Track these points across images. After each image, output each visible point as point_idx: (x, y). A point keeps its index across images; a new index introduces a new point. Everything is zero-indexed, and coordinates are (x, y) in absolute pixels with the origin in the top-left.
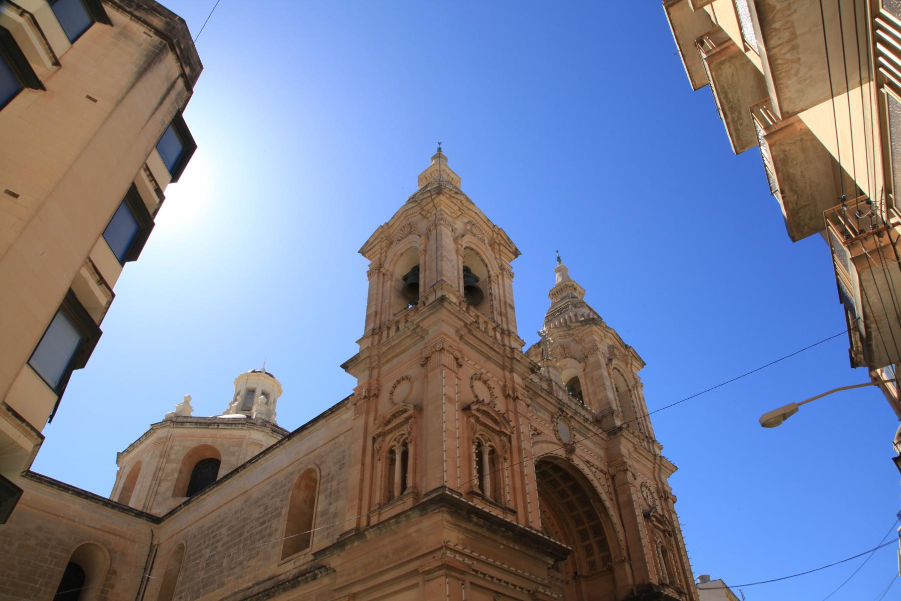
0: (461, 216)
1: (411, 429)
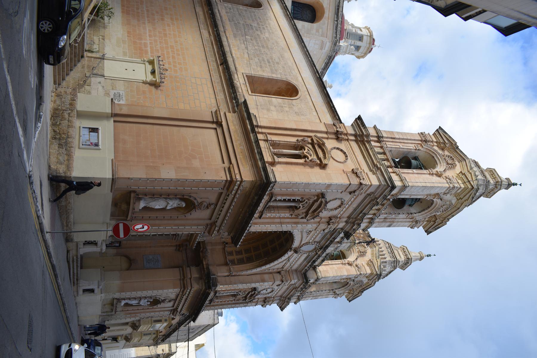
0: (456, 199)
1: (313, 162)
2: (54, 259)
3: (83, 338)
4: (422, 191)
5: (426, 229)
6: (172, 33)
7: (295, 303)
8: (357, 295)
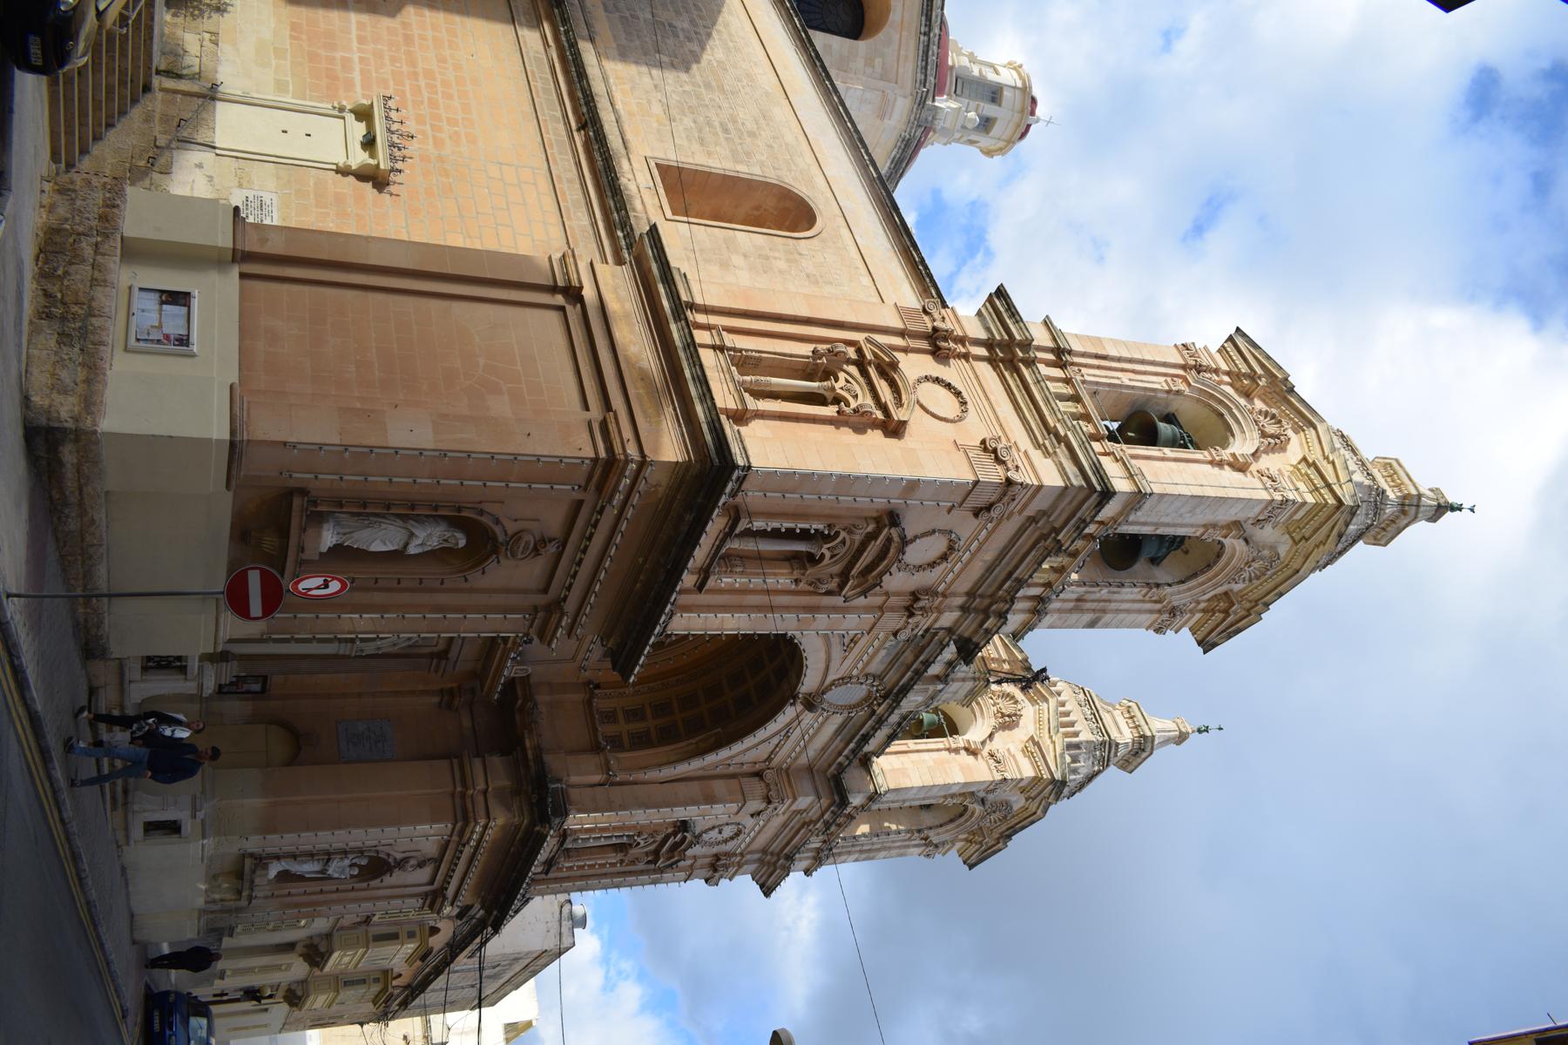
0: (1290, 542)
2: (35, 693)
3: (150, 988)
4: (1192, 511)
5: (1200, 635)
6: (429, 33)
7: (808, 872)
8: (994, 846)
